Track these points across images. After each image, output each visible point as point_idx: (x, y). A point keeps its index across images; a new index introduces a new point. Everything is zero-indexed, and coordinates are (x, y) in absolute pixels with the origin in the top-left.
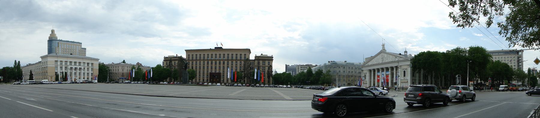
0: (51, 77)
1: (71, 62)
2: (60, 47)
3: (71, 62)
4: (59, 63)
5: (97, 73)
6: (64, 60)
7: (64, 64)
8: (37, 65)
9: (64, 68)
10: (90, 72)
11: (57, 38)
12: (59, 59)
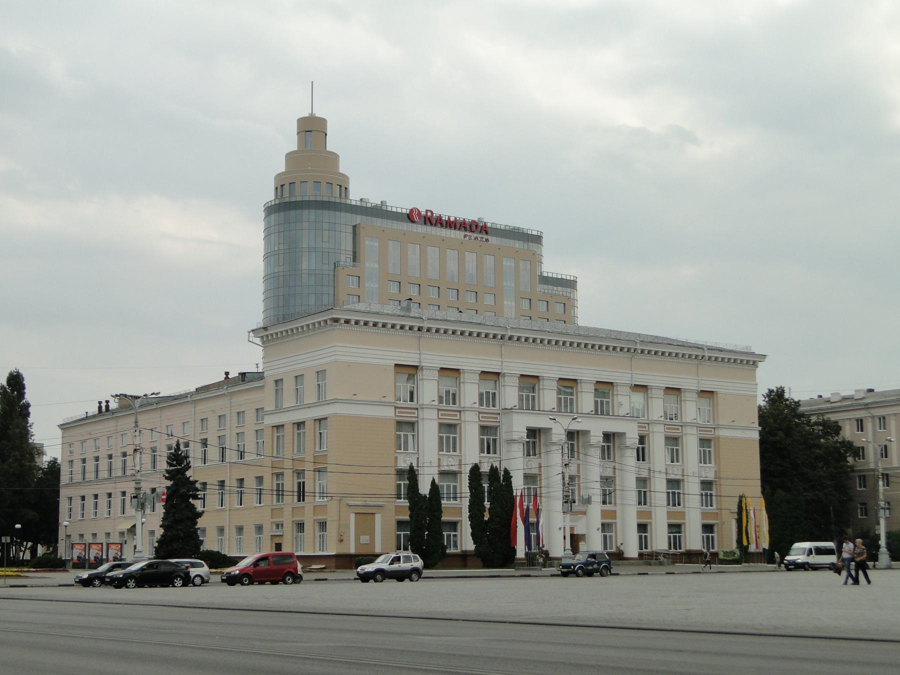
0: (365, 517)
1: (530, 382)
2: (370, 264)
3: (530, 382)
4: (429, 390)
5: (744, 474)
6: (473, 360)
7: (470, 393)
8: (210, 408)
9: (470, 437)
10: (693, 468)
11: (344, 190)
12: (433, 356)
